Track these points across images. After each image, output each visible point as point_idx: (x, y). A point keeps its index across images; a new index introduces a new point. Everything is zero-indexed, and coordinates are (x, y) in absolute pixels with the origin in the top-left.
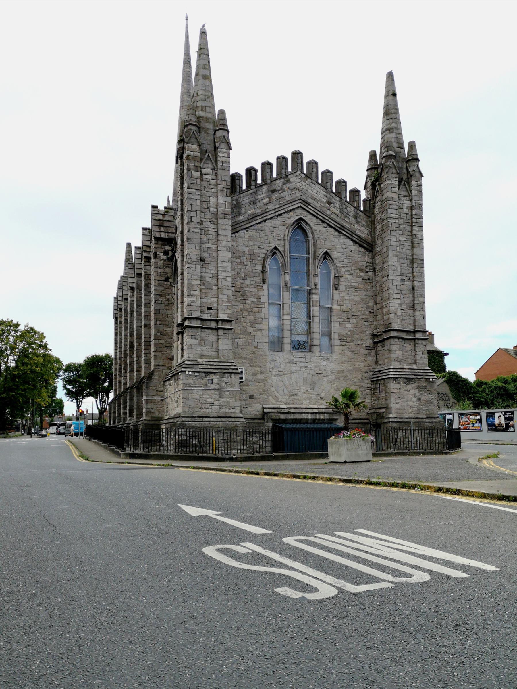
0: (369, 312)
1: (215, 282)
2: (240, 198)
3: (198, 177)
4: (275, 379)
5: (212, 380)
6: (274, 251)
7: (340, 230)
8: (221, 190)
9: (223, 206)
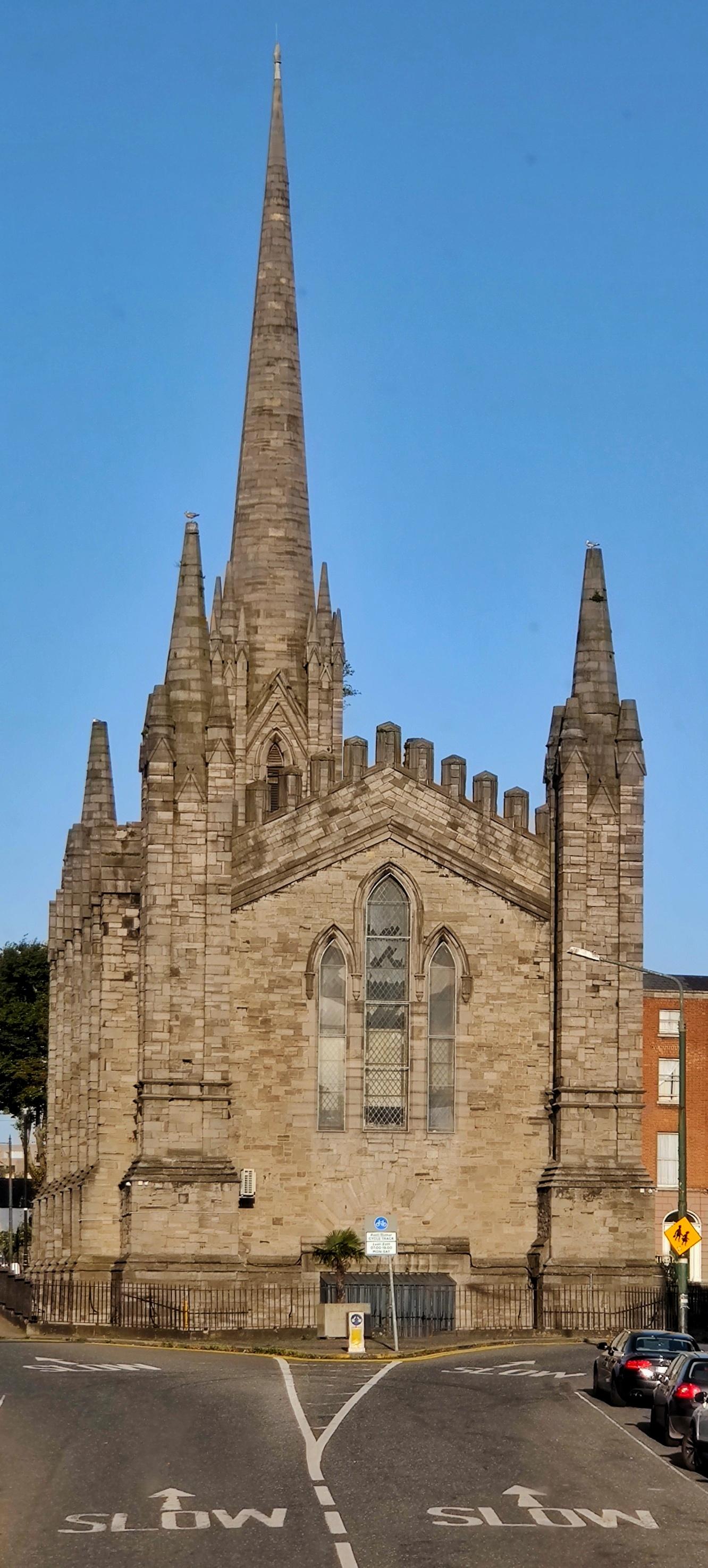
0: (539, 1045)
1: (199, 1013)
2: (262, 832)
3: (169, 820)
4: (327, 1189)
5: (187, 1195)
6: (331, 932)
7: (478, 876)
8: (212, 841)
9: (217, 870)
